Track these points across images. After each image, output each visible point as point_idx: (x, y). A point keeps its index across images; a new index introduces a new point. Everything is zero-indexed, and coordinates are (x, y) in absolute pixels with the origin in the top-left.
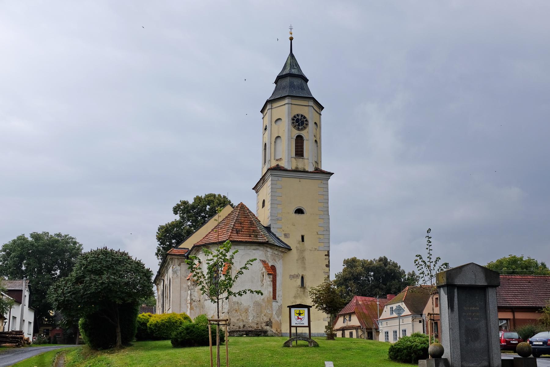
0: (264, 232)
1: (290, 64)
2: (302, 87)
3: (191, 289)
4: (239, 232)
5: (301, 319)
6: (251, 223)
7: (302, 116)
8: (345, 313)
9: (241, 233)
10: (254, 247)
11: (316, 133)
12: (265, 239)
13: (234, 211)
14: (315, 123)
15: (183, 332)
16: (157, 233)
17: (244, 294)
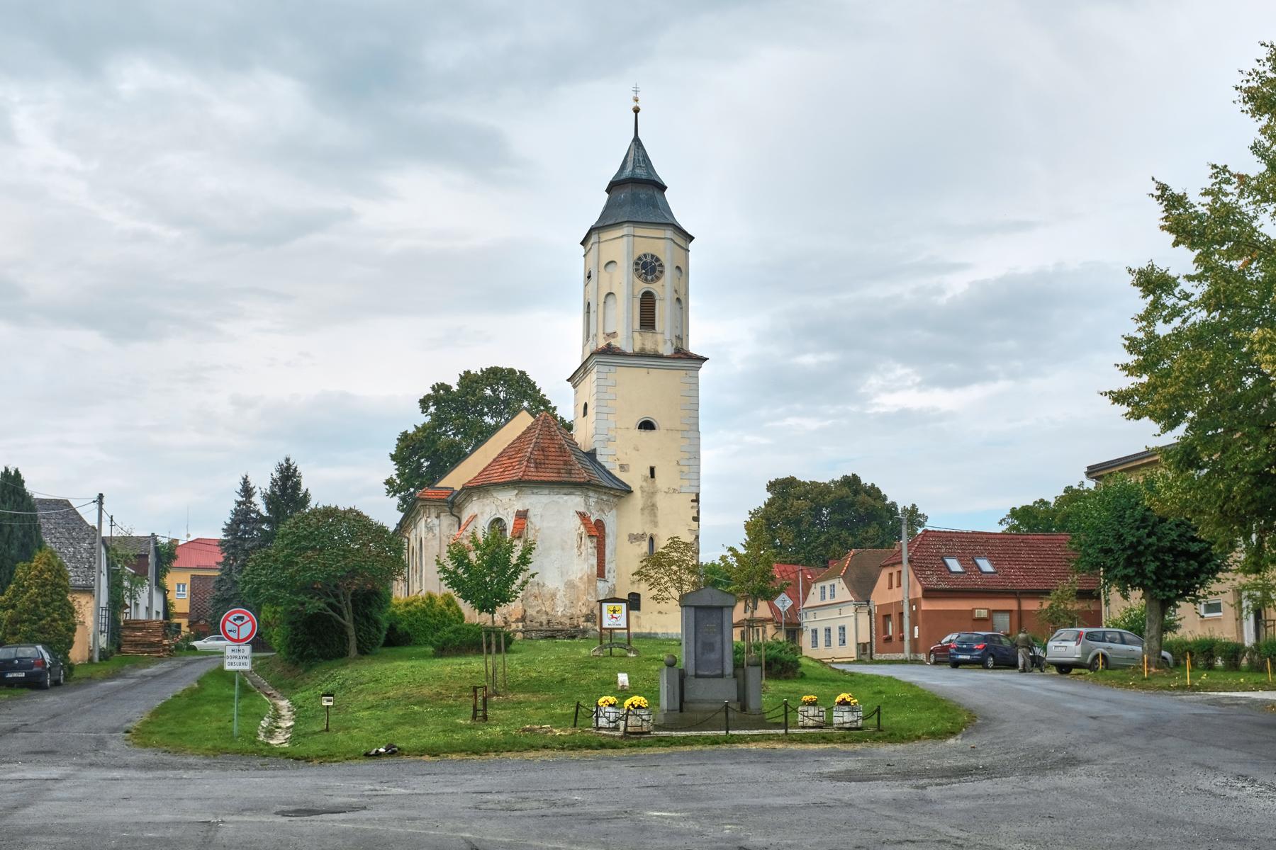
7: (653, 256)
10: (565, 491)
12: (583, 476)
14: (678, 268)
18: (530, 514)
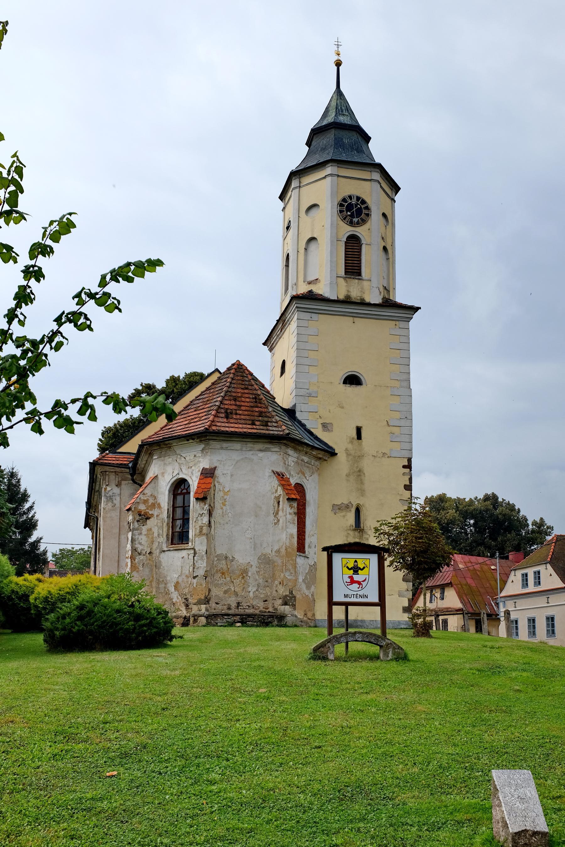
0: (283, 417)
1: (337, 108)
2: (358, 148)
3: (134, 529)
4: (230, 416)
5: (359, 583)
6: (257, 399)
7: (358, 198)
8: (434, 585)
9: (234, 417)
11: (386, 233)
12: (283, 430)
13: (222, 377)
14: (384, 215)
15: (69, 614)
16: (100, 440)
17: (84, 419)
18: (218, 472)
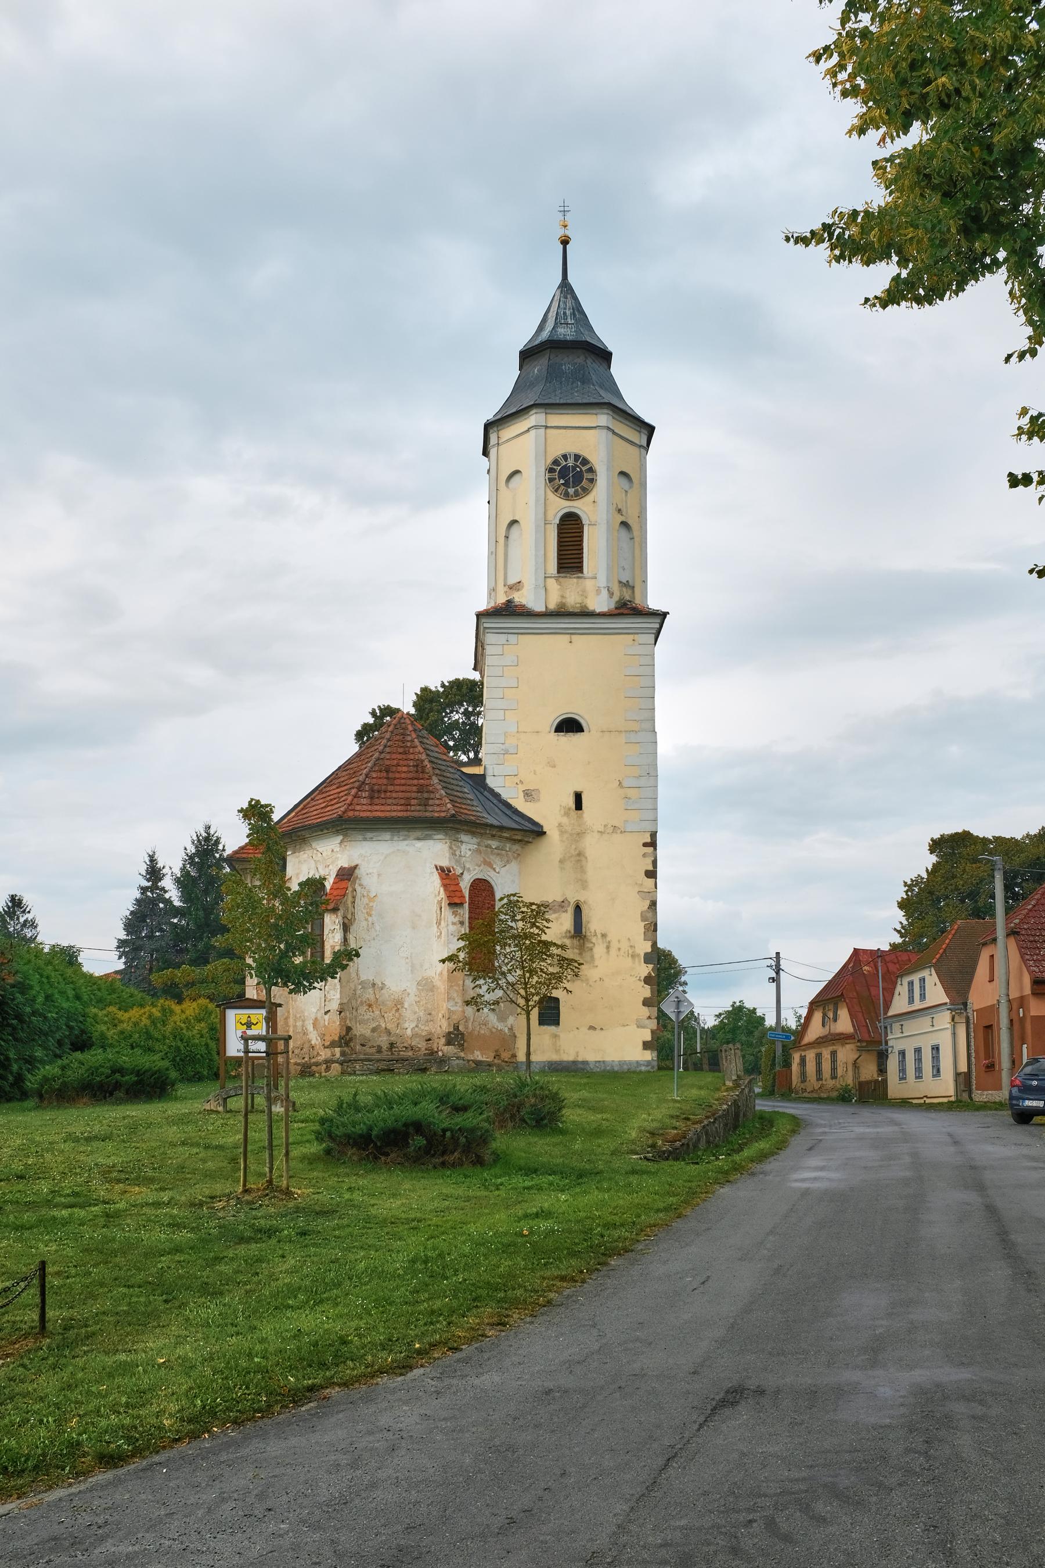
7: (577, 457)
10: (418, 834)
14: (623, 474)
